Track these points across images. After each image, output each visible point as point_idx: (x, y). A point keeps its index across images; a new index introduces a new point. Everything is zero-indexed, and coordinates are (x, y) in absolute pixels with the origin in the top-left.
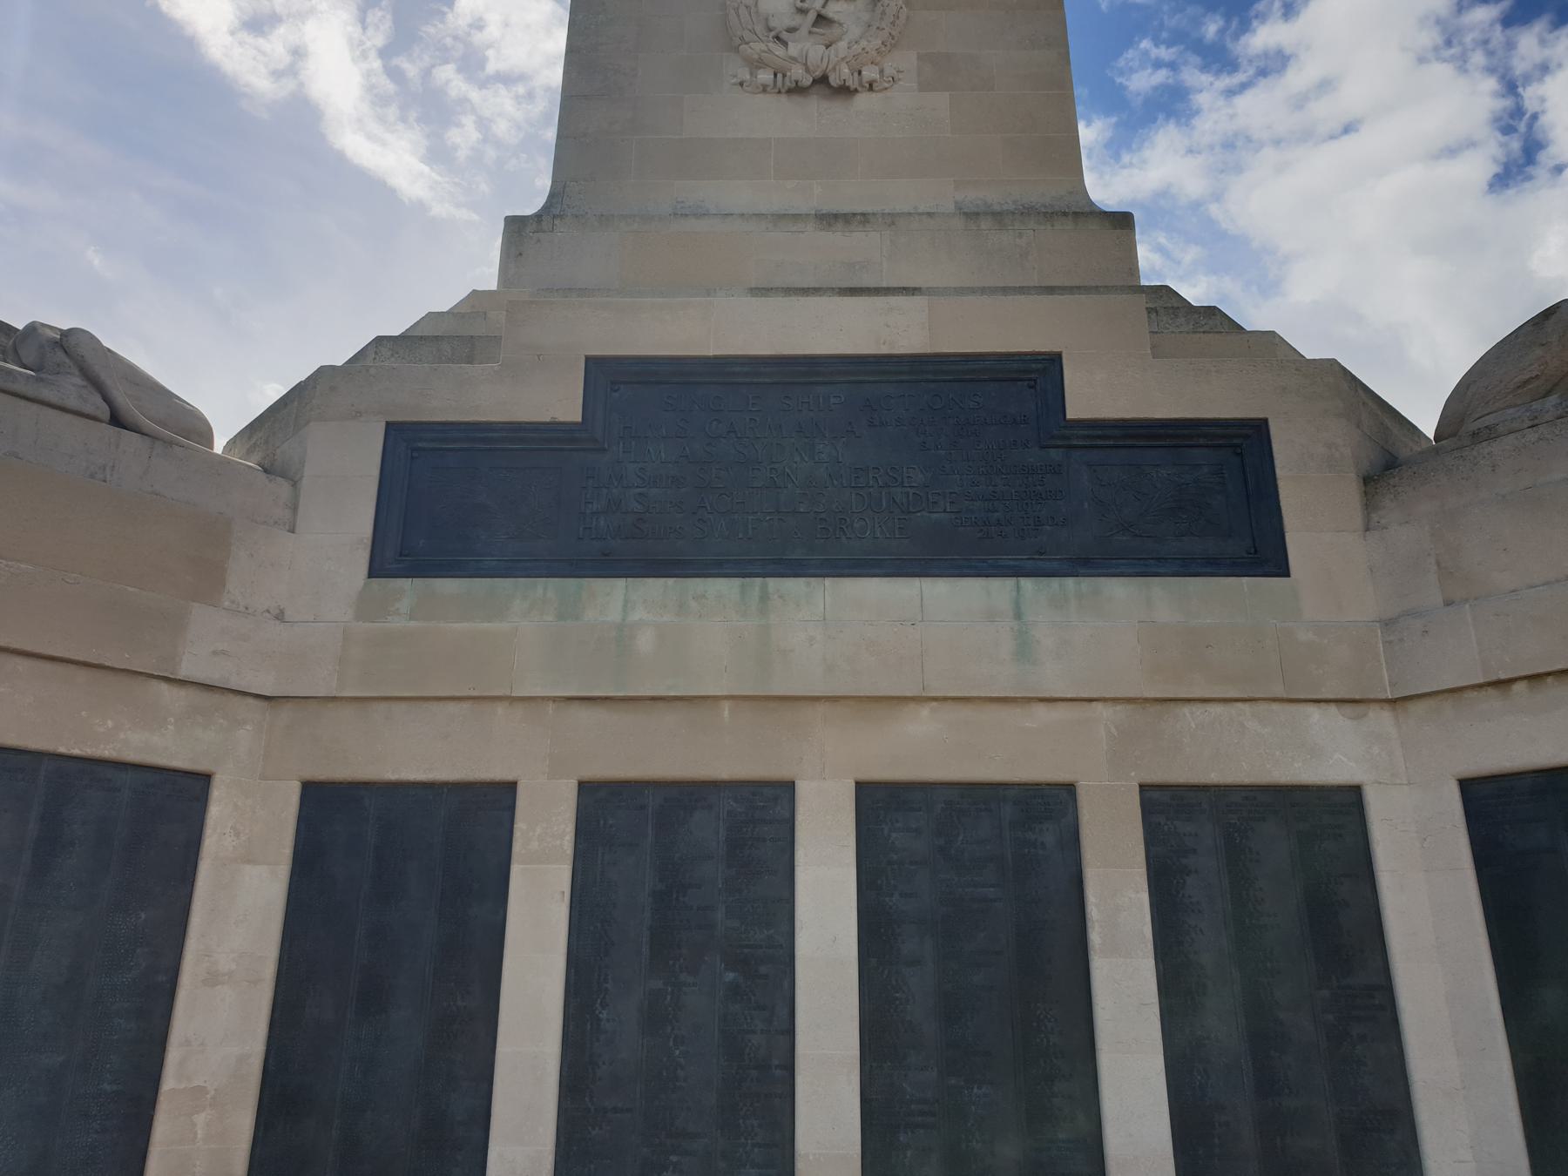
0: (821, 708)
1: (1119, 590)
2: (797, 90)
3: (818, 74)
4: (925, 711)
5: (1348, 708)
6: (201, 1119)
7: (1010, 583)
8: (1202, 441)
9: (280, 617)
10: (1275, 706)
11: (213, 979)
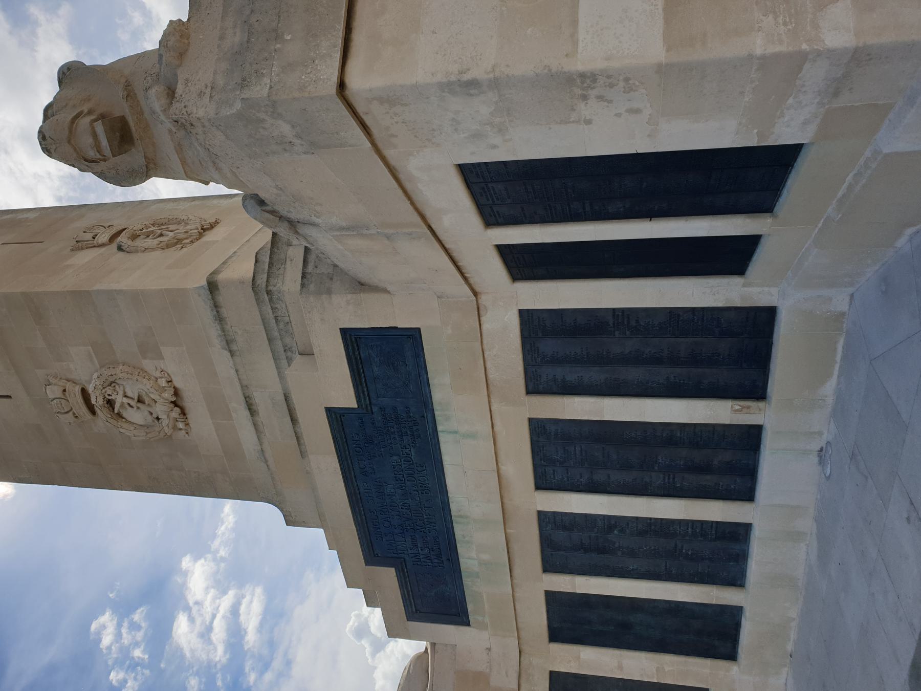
0: (505, 501)
1: (438, 395)
2: (183, 413)
3: (172, 405)
4: (503, 468)
5: (482, 312)
6: (667, 669)
7: (440, 434)
8: (357, 353)
9: (489, 649)
10: (485, 342)
11: (620, 667)
